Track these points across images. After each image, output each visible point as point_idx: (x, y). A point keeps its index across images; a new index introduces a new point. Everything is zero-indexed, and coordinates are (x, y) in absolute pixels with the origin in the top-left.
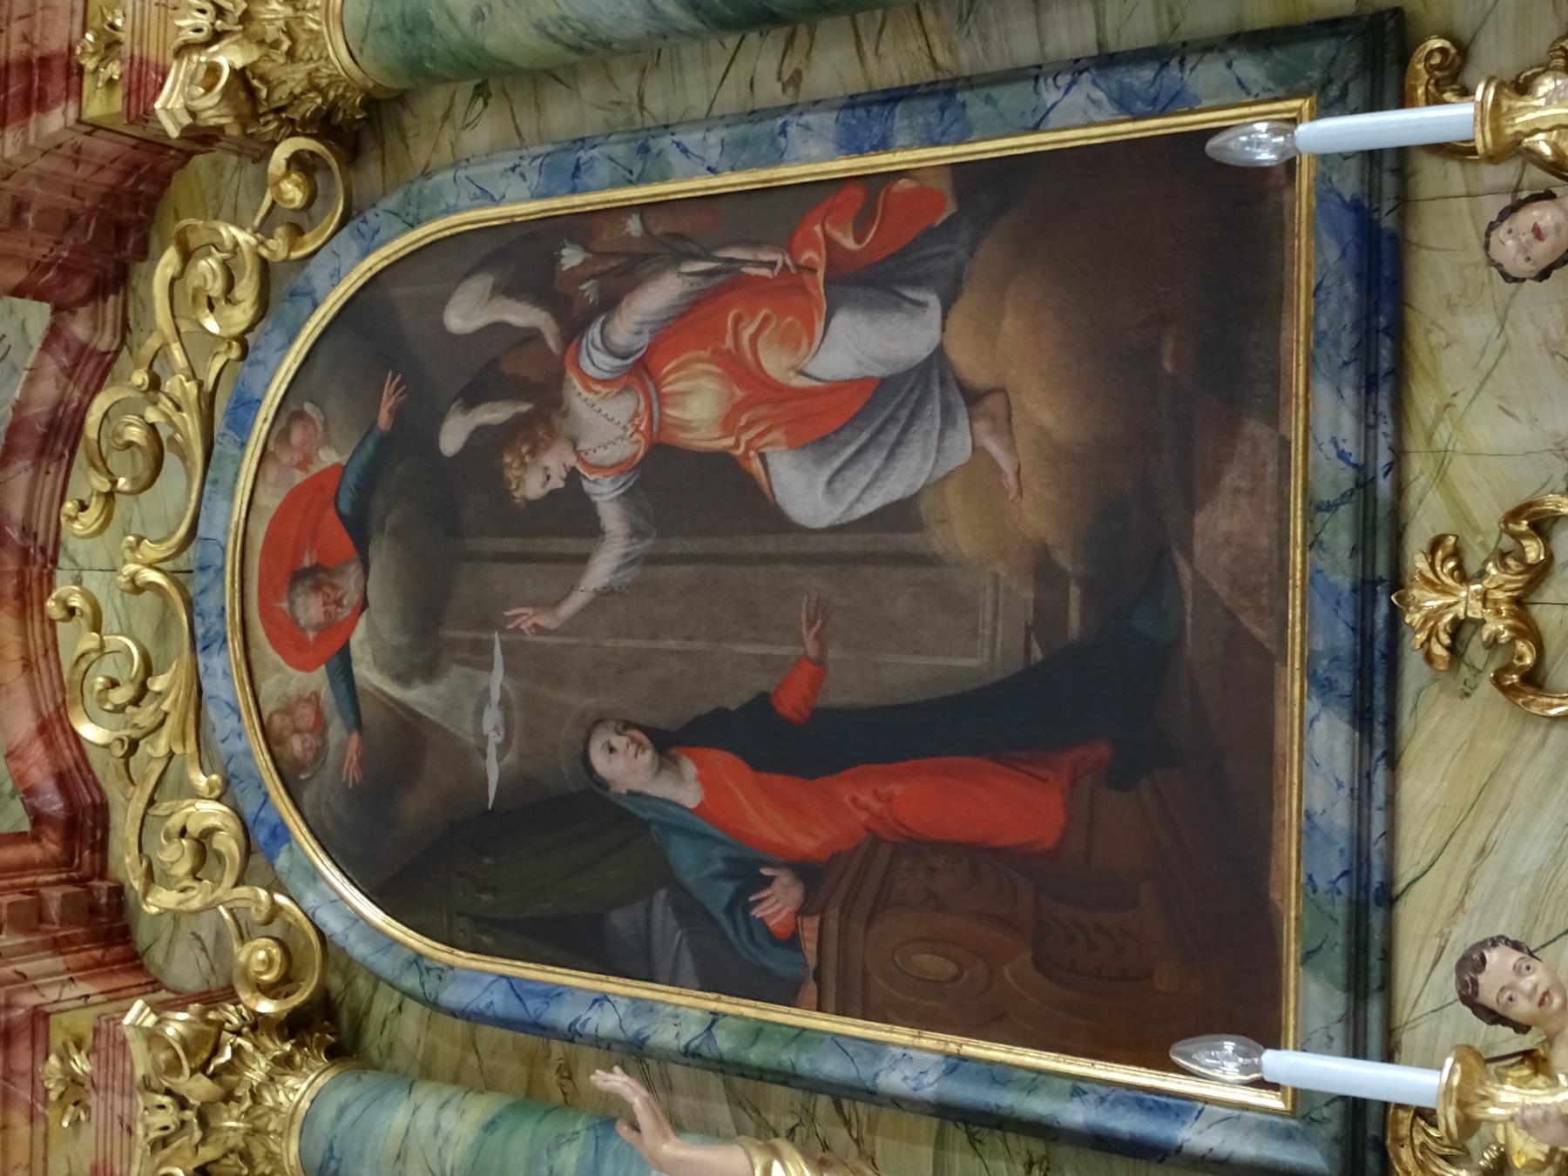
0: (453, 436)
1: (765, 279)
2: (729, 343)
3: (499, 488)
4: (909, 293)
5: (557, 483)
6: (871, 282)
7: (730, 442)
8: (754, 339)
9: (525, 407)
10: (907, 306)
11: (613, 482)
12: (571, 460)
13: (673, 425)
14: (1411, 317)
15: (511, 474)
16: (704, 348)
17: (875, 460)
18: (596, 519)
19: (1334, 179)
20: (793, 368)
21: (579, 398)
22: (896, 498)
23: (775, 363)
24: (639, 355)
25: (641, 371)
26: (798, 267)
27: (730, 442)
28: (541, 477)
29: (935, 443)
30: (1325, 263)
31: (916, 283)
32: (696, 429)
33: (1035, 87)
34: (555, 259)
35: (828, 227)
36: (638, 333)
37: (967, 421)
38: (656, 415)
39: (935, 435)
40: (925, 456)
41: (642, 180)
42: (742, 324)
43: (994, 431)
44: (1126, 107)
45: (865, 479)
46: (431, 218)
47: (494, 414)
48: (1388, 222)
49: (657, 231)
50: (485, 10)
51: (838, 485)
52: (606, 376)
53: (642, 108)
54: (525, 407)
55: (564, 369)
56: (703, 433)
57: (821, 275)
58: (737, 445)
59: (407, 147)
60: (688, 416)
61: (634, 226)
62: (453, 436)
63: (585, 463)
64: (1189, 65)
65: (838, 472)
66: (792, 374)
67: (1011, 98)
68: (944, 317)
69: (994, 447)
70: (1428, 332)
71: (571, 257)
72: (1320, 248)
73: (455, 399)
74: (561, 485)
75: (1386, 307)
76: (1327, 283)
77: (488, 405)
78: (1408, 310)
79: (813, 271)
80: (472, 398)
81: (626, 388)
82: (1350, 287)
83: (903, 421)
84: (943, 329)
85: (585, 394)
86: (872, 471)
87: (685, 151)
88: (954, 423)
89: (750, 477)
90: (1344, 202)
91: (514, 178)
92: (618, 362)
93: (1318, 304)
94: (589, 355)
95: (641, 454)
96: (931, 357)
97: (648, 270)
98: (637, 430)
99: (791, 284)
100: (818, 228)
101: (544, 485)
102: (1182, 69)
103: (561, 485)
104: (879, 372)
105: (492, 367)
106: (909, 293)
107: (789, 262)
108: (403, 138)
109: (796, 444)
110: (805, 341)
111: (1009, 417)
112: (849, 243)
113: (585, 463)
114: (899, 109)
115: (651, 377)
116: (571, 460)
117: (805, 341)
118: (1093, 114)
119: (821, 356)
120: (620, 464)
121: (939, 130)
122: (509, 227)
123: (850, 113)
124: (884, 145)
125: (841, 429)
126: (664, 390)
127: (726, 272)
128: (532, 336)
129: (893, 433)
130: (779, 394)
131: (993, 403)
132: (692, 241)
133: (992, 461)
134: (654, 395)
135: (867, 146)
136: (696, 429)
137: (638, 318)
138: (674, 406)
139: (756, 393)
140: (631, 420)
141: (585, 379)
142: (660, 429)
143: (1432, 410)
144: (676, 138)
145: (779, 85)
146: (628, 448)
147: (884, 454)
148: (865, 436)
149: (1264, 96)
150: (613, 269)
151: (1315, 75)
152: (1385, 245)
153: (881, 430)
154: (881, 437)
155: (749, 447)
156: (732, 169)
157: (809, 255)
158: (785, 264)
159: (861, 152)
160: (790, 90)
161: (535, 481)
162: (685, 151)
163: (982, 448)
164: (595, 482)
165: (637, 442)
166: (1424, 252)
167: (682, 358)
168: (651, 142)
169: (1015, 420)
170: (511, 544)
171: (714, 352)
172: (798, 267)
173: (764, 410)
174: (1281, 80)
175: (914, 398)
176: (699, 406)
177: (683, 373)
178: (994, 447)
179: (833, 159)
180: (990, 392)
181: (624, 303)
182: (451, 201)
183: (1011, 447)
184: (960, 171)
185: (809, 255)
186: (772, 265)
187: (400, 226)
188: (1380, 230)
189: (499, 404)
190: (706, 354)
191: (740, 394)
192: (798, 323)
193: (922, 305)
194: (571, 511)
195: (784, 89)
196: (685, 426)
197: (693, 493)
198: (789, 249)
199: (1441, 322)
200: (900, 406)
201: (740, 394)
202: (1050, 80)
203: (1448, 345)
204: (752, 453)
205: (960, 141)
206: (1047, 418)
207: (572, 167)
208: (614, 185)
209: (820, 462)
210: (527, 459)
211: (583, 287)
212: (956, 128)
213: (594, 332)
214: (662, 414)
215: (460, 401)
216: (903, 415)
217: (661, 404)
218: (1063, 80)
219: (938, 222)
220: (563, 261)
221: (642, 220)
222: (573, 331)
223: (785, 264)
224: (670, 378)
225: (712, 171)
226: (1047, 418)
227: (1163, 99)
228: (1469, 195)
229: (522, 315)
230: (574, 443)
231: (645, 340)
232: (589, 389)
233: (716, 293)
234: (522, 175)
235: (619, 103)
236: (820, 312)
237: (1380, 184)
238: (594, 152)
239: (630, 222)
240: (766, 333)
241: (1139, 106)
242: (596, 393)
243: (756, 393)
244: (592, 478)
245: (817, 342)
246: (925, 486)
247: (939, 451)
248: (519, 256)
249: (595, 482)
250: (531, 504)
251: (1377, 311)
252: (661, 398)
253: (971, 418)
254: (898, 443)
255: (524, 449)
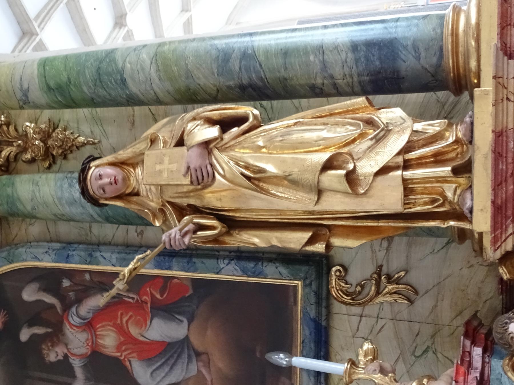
0: (25, 335)
1: (130, 303)
2: (119, 322)
3: (41, 357)
4: (177, 316)
5: (60, 358)
6: (166, 310)
7: (119, 354)
8: (127, 322)
9: (49, 330)
10: (177, 320)
11: (80, 360)
12: (66, 351)
13: (101, 346)
14: (331, 350)
15: (45, 352)
16: (111, 321)
17: (166, 369)
18: (74, 372)
19: (308, 309)
20: (140, 334)
21: (69, 331)
22: (173, 382)
23: (134, 331)
24: (89, 320)
25: (89, 325)
26: (142, 301)
27: (119, 354)
28: (55, 355)
29: (186, 367)
30: (305, 334)
31: (179, 313)
32: (108, 348)
33: (217, 262)
34: (60, 283)
35: (151, 290)
36: (88, 312)
37: (196, 361)
38: (94, 341)
39: (186, 364)
40: (182, 370)
41: (90, 263)
42: (124, 316)
43: (204, 366)
44: (245, 272)
45: (163, 375)
46: (17, 261)
47: (39, 330)
48: (324, 323)
49: (96, 280)
50: (36, 207)
51: (154, 375)
52: (78, 325)
53: (91, 231)
54: (49, 330)
55: (63, 320)
56: (110, 350)
57: (149, 305)
58: (121, 356)
59: (10, 227)
60: (105, 343)
61: (87, 277)
62: (25, 335)
63: (70, 353)
64: (264, 266)
65: (154, 370)
66: (139, 336)
67: (210, 263)
68: (189, 326)
69: (204, 371)
70: (336, 355)
71: (66, 283)
72: (303, 329)
73: (25, 323)
74: (62, 358)
75: (323, 350)
76: (306, 341)
77: (38, 327)
78: (330, 347)
79: (147, 303)
80: (31, 324)
81: (84, 330)
82: (312, 345)
83: (175, 358)
84: (188, 330)
85: (70, 330)
86: (165, 372)
87: (104, 258)
88: (192, 362)
89: (125, 368)
90: (311, 318)
91: (47, 256)
92: (82, 321)
93: (303, 347)
94: (72, 317)
95: (89, 353)
96: (184, 339)
97: (92, 292)
98: (88, 345)
99: (139, 306)
100: (148, 289)
101: (56, 357)
102: (262, 266)
103: (62, 358)
104: (167, 340)
105: (37, 314)
106: (177, 316)
107: (138, 298)
108: (8, 224)
109: (141, 359)
110: (144, 325)
111: (209, 363)
112: (158, 296)
113: (70, 353)
114: (174, 260)
115: (93, 328)
116: (66, 351)
117: (144, 325)
118: (235, 273)
119: (149, 332)
120: (82, 355)
121: (187, 267)
122: (45, 269)
123: (158, 258)
124: (169, 268)
125: (155, 357)
126: (97, 333)
127: (118, 298)
128: (52, 307)
129: (172, 361)
130: (134, 341)
131: (204, 357)
132: (107, 285)
133: (203, 375)
134: (94, 335)
135: (164, 268)
136: (108, 348)
137: (89, 308)
138: (100, 339)
139: (127, 340)
140: (86, 341)
141: (70, 323)
142: (96, 346)
143: (337, 379)
144: (101, 254)
145: (136, 234)
146: (85, 350)
147: (169, 367)
148: (163, 360)
149: (287, 278)
150: (80, 289)
151: (302, 275)
152: (323, 330)
153: (168, 359)
154: (168, 362)
155: (125, 356)
156: (120, 266)
157: (145, 297)
158: (137, 299)
159: (162, 269)
160: (140, 236)
161: (53, 355)
162: (104, 258)
163: (200, 371)
164: (74, 360)
165: (88, 349)
166: (335, 330)
167: (104, 323)
168: (93, 253)
169: (211, 363)
170: (44, 376)
171: (114, 324)
172: (142, 301)
173: (131, 346)
174: (292, 275)
175: (179, 350)
176: (109, 341)
177: (103, 329)
178: (204, 371)
179: (153, 269)
180: (204, 353)
181: (84, 301)
182: (25, 257)
183: (209, 372)
184: (194, 281)
185: (145, 297)
186: (133, 298)
187: (7, 262)
188: (321, 325)
189: (41, 327)
190: (111, 324)
191: (122, 339)
192: (142, 319)
193: (181, 321)
194: (64, 366)
195: (138, 236)
196: (104, 346)
197: (96, 360)
198: (138, 294)
199: (339, 353)
200: (174, 353)
201: (122, 339)
202: (222, 261)
203: (341, 360)
204: (126, 359)
205: (194, 272)
206: (221, 365)
207: (66, 256)
208: (80, 263)
209: (149, 366)
210: (50, 348)
211: (70, 294)
212: (192, 268)
213: (74, 309)
214: (96, 340)
215: (27, 324)
216: (176, 355)
217: (96, 337)
218: (226, 261)
219: (187, 295)
220: (63, 284)
221: (90, 275)
222: (67, 308)
223: (137, 299)
224: (99, 330)
225: (113, 265)
226: (221, 365)
227: (257, 273)
228: (348, 315)
229: (49, 299)
230: (66, 345)
231: (90, 315)
232: (72, 328)
233: (115, 304)
234: (49, 255)
235: (82, 228)
236: (149, 316)
237: (322, 311)
238: (74, 253)
239: (86, 275)
240: (131, 321)
241: (249, 273)
242: (74, 330)
243: (127, 340)
244: (73, 358)
245: (148, 326)
246: (182, 380)
247: (187, 369)
248: (49, 279)
249: (74, 360)
250: (52, 363)
251: (321, 351)
252: (96, 336)
253: (197, 361)
254: (174, 364)
255: (49, 344)
